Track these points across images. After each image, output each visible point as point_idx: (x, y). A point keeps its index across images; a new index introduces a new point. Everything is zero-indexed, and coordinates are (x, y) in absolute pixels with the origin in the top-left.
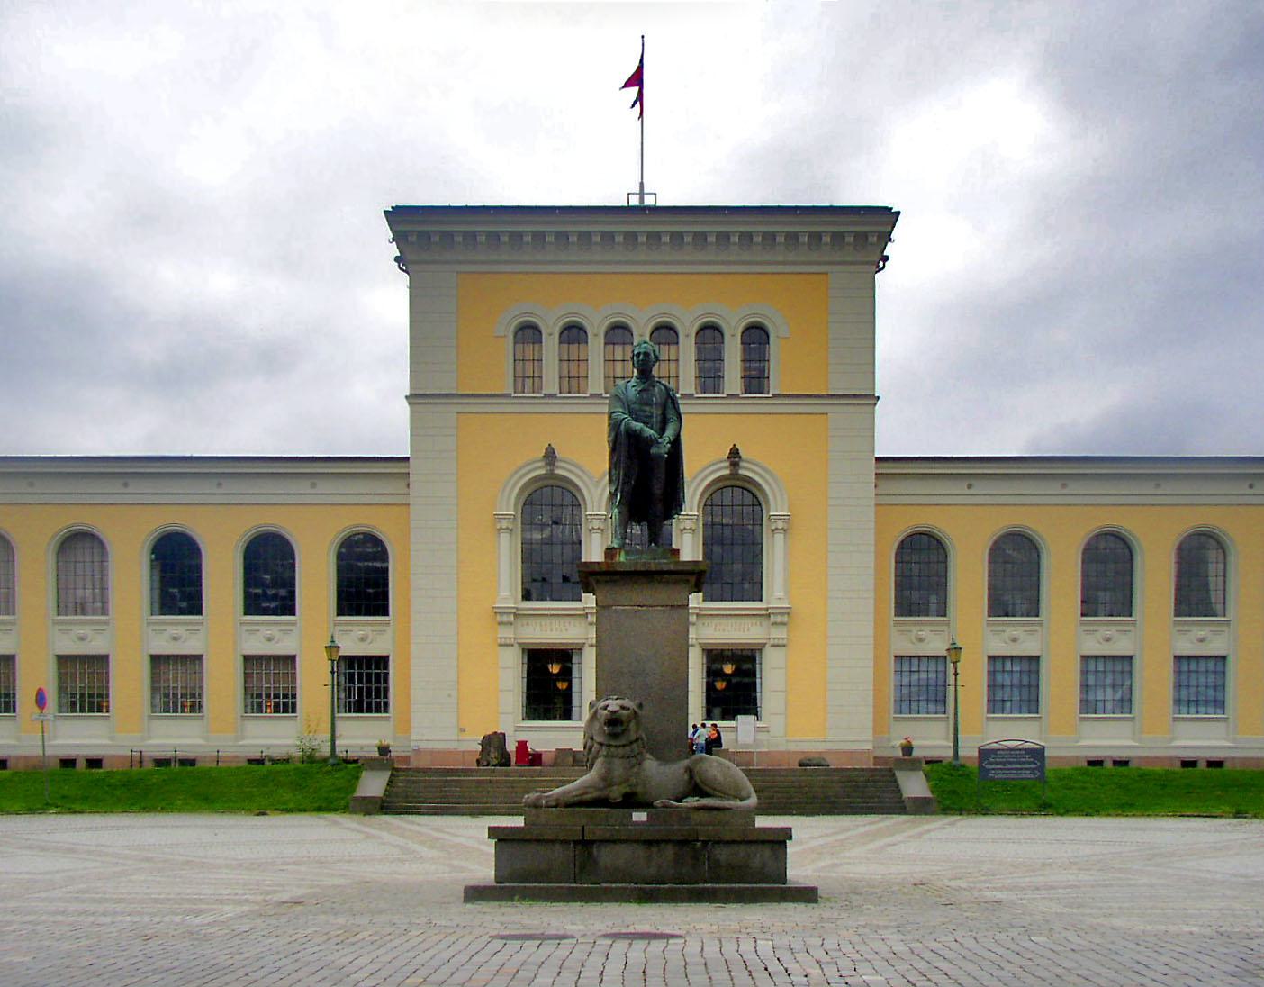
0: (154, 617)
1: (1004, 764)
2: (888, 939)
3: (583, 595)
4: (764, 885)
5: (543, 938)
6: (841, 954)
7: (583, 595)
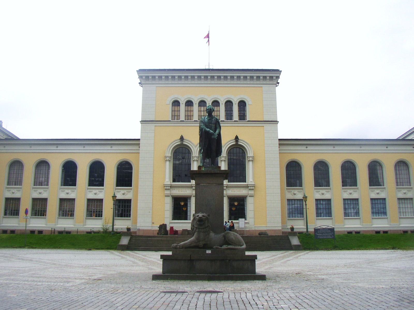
1: (322, 233)
2: (289, 292)
3: (191, 180)
4: (249, 275)
5: (177, 292)
7: (191, 180)
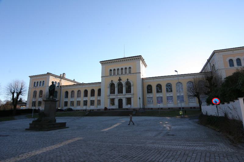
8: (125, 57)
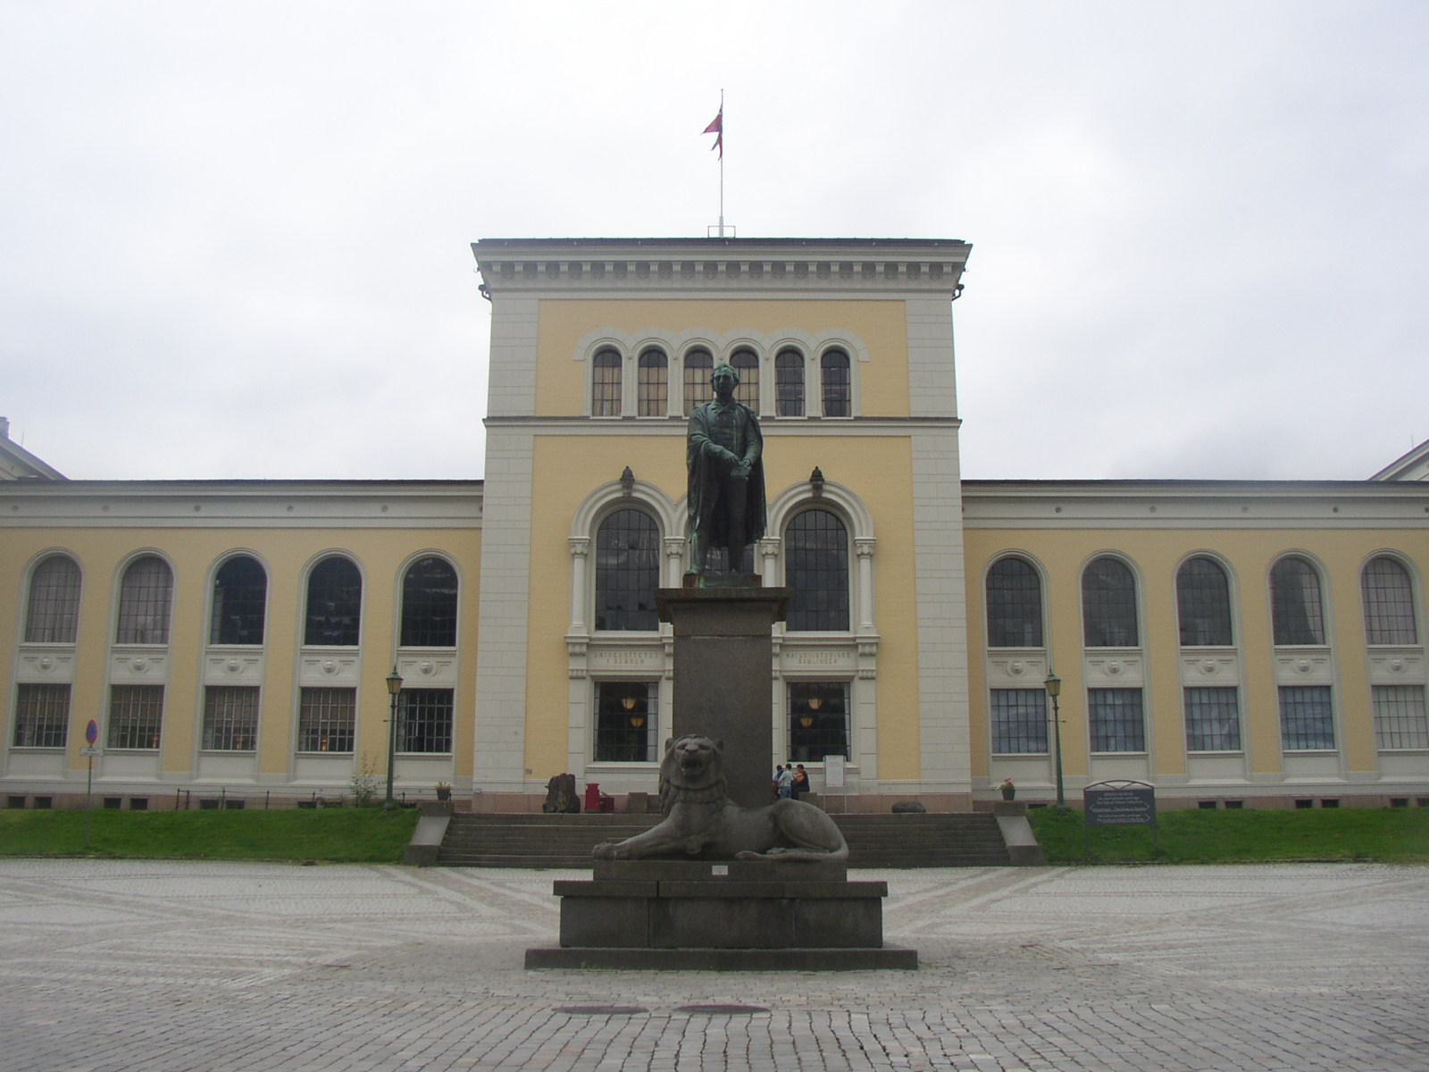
0: (213, 646)
1: (1112, 807)
2: (997, 1010)
3: (660, 624)
4: (858, 949)
5: (612, 1011)
6: (944, 1029)
7: (660, 624)
8: (728, 234)
